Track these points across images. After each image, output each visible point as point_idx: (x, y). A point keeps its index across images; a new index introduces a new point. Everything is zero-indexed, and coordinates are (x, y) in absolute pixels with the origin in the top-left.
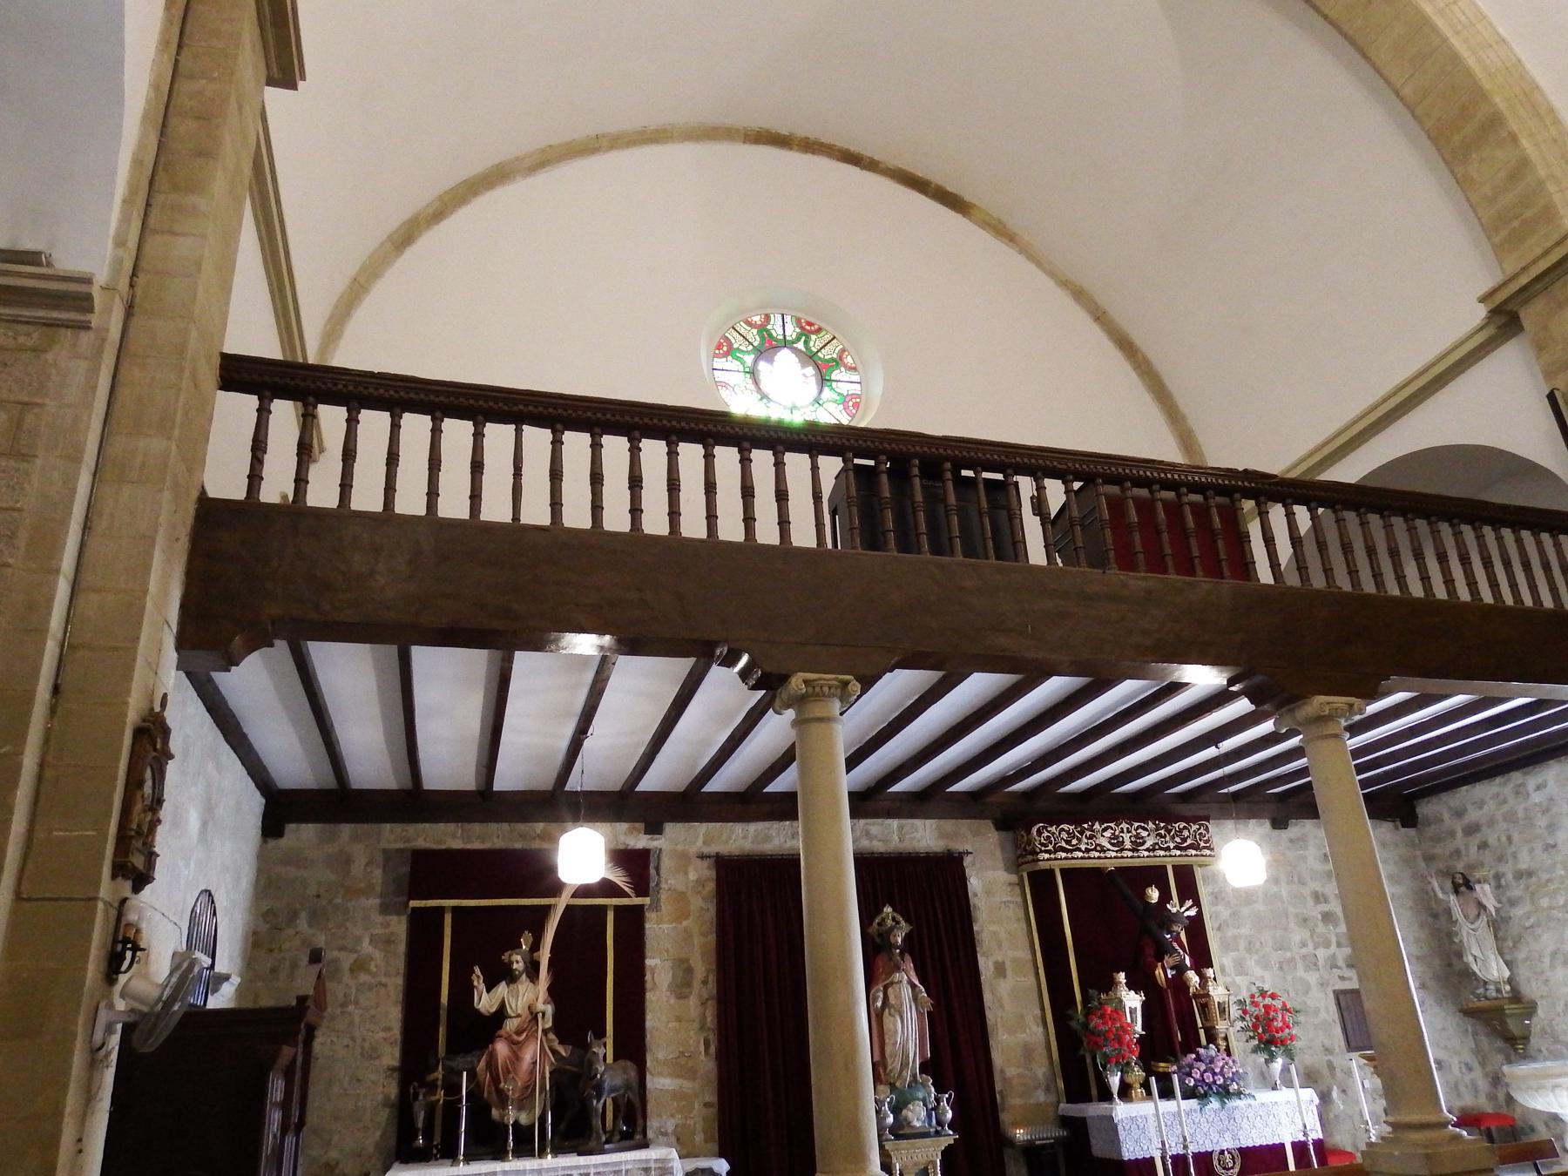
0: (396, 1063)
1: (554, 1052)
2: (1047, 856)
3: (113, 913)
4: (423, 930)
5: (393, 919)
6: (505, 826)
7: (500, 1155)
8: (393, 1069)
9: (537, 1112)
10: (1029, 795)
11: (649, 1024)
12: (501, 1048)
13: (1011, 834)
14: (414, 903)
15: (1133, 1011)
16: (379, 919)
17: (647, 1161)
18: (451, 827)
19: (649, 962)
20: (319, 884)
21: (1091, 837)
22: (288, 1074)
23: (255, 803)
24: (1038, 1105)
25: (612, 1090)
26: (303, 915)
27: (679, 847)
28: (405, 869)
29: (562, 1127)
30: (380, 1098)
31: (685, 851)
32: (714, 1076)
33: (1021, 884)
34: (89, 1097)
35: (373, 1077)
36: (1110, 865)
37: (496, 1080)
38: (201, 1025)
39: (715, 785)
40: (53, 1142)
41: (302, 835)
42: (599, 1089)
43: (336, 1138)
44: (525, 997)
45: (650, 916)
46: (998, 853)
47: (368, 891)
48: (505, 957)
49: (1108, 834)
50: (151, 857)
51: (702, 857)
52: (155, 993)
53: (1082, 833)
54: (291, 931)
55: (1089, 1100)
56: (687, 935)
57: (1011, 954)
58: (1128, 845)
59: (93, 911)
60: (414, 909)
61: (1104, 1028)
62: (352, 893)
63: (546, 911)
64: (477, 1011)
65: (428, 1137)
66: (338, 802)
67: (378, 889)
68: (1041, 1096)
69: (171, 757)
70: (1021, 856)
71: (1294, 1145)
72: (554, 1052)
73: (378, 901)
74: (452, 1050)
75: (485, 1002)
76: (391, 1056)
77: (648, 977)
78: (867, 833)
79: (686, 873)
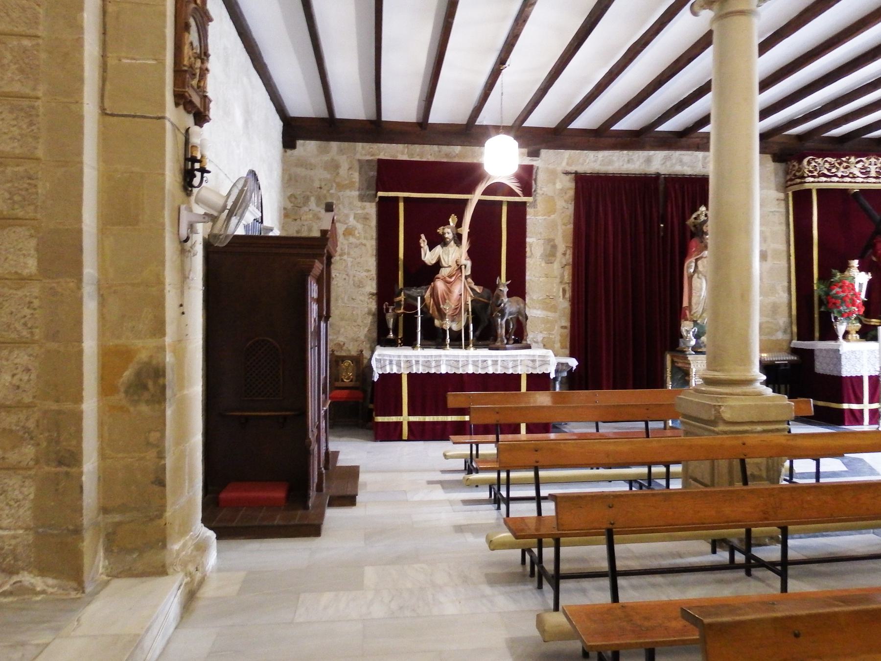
0: (375, 291)
1: (472, 289)
2: (812, 179)
3: (181, 139)
4: (386, 210)
5: (368, 204)
6: (435, 147)
7: (441, 345)
8: (373, 294)
9: (463, 324)
10: (800, 137)
11: (527, 278)
12: (440, 285)
13: (783, 165)
14: (380, 194)
15: (861, 285)
16: (359, 204)
17: (534, 356)
18: (400, 146)
19: (528, 240)
20: (320, 180)
21: (846, 168)
22: (319, 281)
23: (276, 125)
24: (777, 340)
25: (510, 314)
26: (313, 199)
27: (551, 167)
28: (374, 173)
29: (478, 333)
30: (366, 309)
31: (558, 168)
32: (568, 310)
33: (786, 200)
34: (184, 277)
35: (361, 298)
36: (856, 187)
37: (437, 304)
38: (256, 246)
39: (578, 124)
40: (159, 304)
41: (307, 148)
42: (503, 313)
43: (342, 330)
44: (452, 256)
45: (530, 211)
46: (772, 178)
47: (350, 186)
48: (440, 231)
49: (860, 165)
50: (205, 99)
51: (567, 173)
52: (220, 202)
53: (840, 164)
54: (306, 209)
55: (813, 339)
56: (553, 226)
57: (773, 246)
58: (873, 174)
59: (164, 128)
60: (381, 198)
61: (842, 295)
62: (341, 187)
63: (465, 202)
64: (424, 262)
65: (396, 332)
66: (328, 128)
67: (357, 185)
68: (780, 336)
69: (211, 20)
70: (791, 180)
71: (870, 377)
72: (472, 289)
73: (357, 193)
74: (408, 284)
75: (429, 257)
76: (372, 286)
77: (528, 249)
78: (681, 161)
79: (554, 184)
